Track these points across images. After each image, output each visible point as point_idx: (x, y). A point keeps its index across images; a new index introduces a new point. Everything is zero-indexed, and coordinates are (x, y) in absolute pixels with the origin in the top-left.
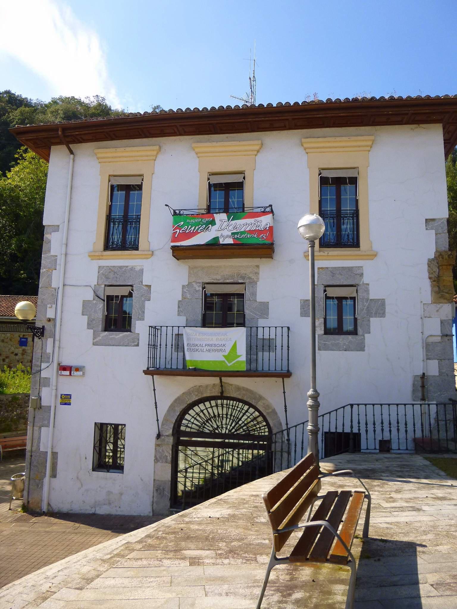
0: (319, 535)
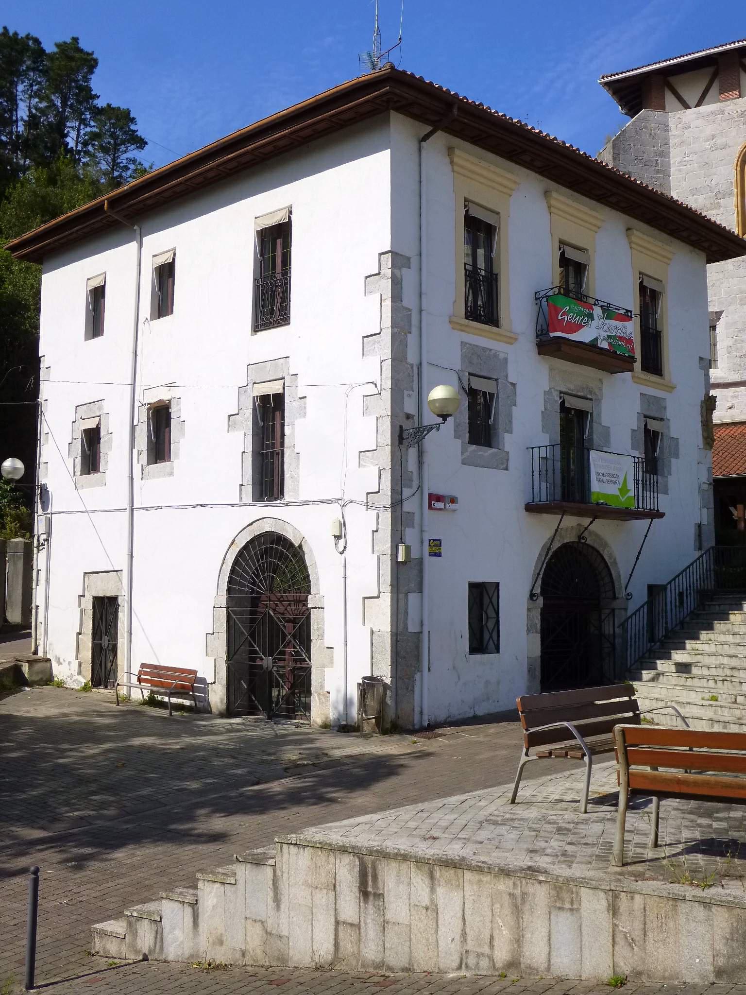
0: (626, 699)
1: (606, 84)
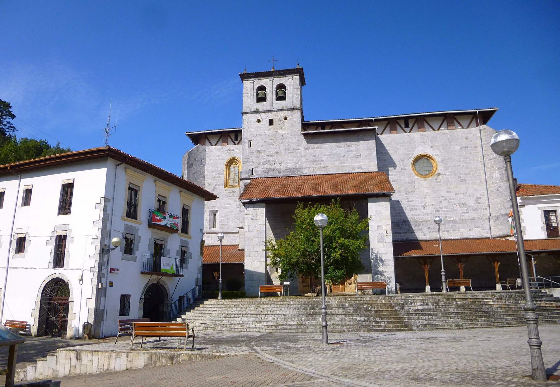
1: (188, 135)
